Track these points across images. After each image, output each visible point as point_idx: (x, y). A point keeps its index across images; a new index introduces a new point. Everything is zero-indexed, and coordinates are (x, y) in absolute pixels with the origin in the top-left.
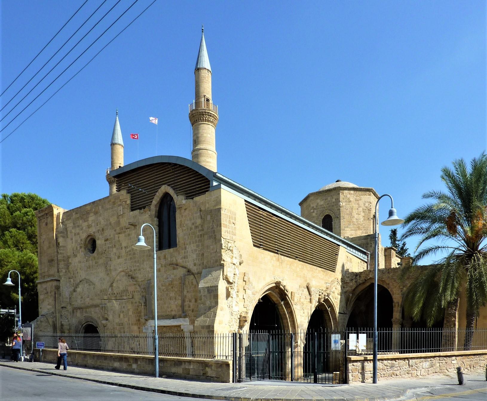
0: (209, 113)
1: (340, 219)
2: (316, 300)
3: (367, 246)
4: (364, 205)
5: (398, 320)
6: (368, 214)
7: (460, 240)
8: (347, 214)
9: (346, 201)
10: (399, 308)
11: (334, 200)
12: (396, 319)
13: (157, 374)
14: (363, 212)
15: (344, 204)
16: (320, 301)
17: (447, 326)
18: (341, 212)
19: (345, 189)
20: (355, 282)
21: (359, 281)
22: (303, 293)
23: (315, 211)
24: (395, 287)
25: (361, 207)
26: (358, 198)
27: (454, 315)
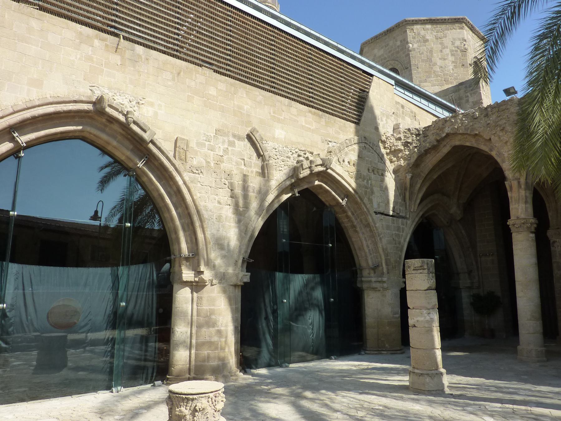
1: (411, 70)
4: (453, 44)
5: (523, 222)
6: (463, 58)
9: (419, 41)
10: (523, 192)
11: (398, 43)
12: (518, 218)
13: (198, 318)
14: (452, 55)
15: (416, 46)
16: (298, 175)
18: (411, 57)
19: (415, 23)
21: (424, 144)
22: (230, 148)
24: (506, 143)
25: (447, 48)
26: (440, 34)
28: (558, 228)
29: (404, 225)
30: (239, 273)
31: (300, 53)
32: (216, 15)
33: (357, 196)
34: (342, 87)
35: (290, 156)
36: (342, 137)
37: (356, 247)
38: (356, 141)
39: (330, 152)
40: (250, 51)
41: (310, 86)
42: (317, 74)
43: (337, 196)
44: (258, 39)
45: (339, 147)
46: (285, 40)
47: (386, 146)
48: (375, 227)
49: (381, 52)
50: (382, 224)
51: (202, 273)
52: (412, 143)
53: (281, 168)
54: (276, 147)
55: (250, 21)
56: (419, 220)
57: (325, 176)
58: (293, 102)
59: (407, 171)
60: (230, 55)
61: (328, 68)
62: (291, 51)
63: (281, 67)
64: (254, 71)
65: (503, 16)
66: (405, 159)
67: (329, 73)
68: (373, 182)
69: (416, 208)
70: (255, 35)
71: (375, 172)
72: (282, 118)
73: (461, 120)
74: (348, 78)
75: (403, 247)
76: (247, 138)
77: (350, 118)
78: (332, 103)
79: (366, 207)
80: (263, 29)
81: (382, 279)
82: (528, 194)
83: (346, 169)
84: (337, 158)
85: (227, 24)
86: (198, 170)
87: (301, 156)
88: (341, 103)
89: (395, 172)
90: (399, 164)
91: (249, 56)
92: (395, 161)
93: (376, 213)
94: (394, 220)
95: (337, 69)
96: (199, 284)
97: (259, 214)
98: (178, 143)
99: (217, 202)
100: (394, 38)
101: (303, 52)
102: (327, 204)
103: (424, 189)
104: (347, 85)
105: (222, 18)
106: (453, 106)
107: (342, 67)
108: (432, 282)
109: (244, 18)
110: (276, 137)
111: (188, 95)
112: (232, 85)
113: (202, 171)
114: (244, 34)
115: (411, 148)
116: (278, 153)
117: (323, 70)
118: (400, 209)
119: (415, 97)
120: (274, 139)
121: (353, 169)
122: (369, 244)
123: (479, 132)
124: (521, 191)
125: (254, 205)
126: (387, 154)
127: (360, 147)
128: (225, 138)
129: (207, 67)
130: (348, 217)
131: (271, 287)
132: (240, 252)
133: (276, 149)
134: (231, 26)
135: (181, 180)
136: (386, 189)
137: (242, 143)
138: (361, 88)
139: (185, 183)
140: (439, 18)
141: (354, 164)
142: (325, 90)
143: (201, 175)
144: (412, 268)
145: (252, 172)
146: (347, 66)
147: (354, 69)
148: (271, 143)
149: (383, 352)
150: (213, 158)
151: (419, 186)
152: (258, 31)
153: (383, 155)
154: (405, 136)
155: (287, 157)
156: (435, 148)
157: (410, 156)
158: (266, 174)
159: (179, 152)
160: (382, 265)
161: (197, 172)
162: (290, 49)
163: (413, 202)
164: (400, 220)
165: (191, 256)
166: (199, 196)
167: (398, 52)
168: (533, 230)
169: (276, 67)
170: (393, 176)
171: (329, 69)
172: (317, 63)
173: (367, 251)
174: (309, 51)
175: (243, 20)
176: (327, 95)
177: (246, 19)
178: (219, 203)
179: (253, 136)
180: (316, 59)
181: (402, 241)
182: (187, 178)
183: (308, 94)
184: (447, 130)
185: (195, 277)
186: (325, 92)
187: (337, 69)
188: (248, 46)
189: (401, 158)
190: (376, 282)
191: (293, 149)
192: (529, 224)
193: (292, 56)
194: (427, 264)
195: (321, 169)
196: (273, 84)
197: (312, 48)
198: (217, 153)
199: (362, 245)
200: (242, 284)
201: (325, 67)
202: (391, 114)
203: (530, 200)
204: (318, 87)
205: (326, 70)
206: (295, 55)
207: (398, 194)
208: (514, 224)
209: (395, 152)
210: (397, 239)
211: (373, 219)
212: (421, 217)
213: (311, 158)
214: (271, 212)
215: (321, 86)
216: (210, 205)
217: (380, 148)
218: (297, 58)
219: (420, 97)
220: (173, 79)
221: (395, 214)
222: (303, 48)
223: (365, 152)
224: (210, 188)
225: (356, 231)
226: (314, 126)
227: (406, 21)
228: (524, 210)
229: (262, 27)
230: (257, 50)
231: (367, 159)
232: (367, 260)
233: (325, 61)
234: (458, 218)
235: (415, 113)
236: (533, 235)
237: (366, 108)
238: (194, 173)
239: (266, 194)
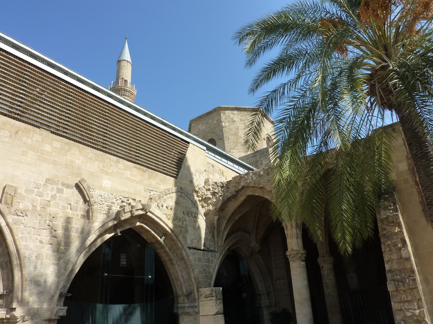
0: (124, 89)
1: (224, 141)
3: (257, 164)
5: (296, 253)
7: (371, 124)
8: (232, 135)
10: (294, 230)
11: (215, 122)
12: (292, 250)
15: (227, 124)
16: (120, 218)
17: (388, 249)
18: (224, 132)
21: (226, 194)
22: (58, 195)
27: (395, 220)
28: (324, 256)
29: (213, 257)
30: (54, 308)
31: (130, 124)
32: (59, 90)
33: (173, 235)
34: (164, 150)
35: (115, 202)
36: (163, 187)
38: (174, 191)
39: (151, 199)
40: (86, 119)
41: (137, 148)
42: (144, 139)
43: (156, 235)
44: (95, 110)
45: (159, 195)
46: (118, 113)
47: (199, 195)
48: (189, 260)
49: (204, 127)
50: (195, 257)
51: (14, 309)
52: (218, 193)
54: (102, 195)
55: (89, 97)
56: (226, 252)
57: (145, 218)
58: (121, 160)
59: (215, 214)
60: (67, 121)
61: (153, 136)
62: (122, 122)
63: (113, 133)
64: (89, 134)
65: (262, 106)
66: (213, 205)
67: (154, 139)
68: (188, 223)
69: (223, 243)
70: (92, 108)
71: (189, 215)
72: (111, 171)
73: (252, 177)
74: (169, 144)
75: (212, 276)
76: (75, 186)
77: (169, 173)
78: (155, 162)
79: (181, 243)
80: (99, 104)
81: (194, 305)
82: (298, 232)
83: (164, 212)
84: (157, 204)
85: (68, 98)
86: (24, 213)
87: (124, 202)
88: (163, 161)
89: (206, 215)
90: (209, 208)
91: (85, 123)
92: (206, 206)
93: (190, 248)
94: (204, 254)
95: (160, 136)
96: (10, 321)
97: (79, 251)
98: (6, 189)
99: (38, 242)
100: (213, 118)
101: (132, 123)
102: (149, 241)
104: (168, 149)
105: (64, 93)
106: (251, 167)
107: (165, 135)
108: (220, 307)
109: (84, 95)
110: (103, 186)
111: (23, 150)
112: (66, 144)
113: (27, 214)
114: (82, 107)
115: (218, 196)
116: (103, 200)
117: (149, 137)
118: (210, 244)
119: (223, 160)
120: (101, 188)
121: (171, 213)
122: (184, 275)
123: (264, 186)
124: (293, 229)
125: (75, 244)
126: (200, 201)
127: (177, 195)
128: (54, 186)
129: (44, 129)
130: (166, 252)
131: (91, 319)
132: (57, 286)
133: (101, 196)
134: (71, 99)
135: (4, 222)
136: (199, 228)
137: (70, 191)
138: (180, 151)
139: (8, 225)
140: (242, 107)
141: (171, 209)
142: (150, 151)
143: (26, 218)
144: (204, 296)
145: (77, 215)
146: (169, 135)
147: (174, 137)
148: (97, 191)
150: (40, 202)
151: (224, 225)
152: (95, 105)
153: (196, 202)
154: (213, 188)
155: (112, 203)
156: (234, 197)
157: (216, 203)
158: (91, 217)
159: (6, 197)
160: (194, 293)
161: (21, 215)
162: (122, 120)
163: (220, 239)
164: (210, 253)
165: (5, 293)
166: (20, 236)
167: (215, 128)
168: (303, 259)
169: (109, 133)
170: (205, 218)
171: (154, 136)
172: (144, 132)
173: (182, 280)
174: (138, 122)
175: (83, 96)
176: (151, 155)
177: (86, 96)
178: (41, 242)
179: (81, 185)
180: (144, 129)
181: (211, 270)
182: (10, 220)
183: (135, 154)
184: (242, 184)
185: (7, 314)
186: (150, 153)
187: (160, 136)
188: (85, 115)
189: (210, 204)
190: (189, 307)
191: (118, 196)
192: (301, 255)
193: (123, 125)
194: (216, 292)
195: (141, 212)
196: (104, 145)
197: (140, 121)
198: (44, 199)
199: (178, 276)
200: (57, 318)
201: (150, 135)
202: (203, 171)
203: (300, 236)
204: (143, 149)
205: (151, 137)
206: (126, 125)
207: (208, 232)
208: (291, 255)
209: (205, 200)
210: (207, 269)
211: (187, 253)
212: (228, 250)
213: (133, 204)
214: (94, 249)
215: (154, 149)
216: (31, 245)
217: (194, 196)
218: (127, 127)
219: (227, 159)
220: (11, 137)
221: (206, 248)
222: (133, 120)
223: (181, 199)
224: (33, 229)
225: (173, 264)
226: (138, 178)
227: (220, 107)
228: (296, 243)
229: (99, 102)
230: (104, 120)
231: (183, 204)
232: (181, 288)
233: (151, 130)
234: (257, 250)
235: (223, 171)
236: (303, 263)
237: (183, 166)
238: (18, 216)
239: (88, 234)
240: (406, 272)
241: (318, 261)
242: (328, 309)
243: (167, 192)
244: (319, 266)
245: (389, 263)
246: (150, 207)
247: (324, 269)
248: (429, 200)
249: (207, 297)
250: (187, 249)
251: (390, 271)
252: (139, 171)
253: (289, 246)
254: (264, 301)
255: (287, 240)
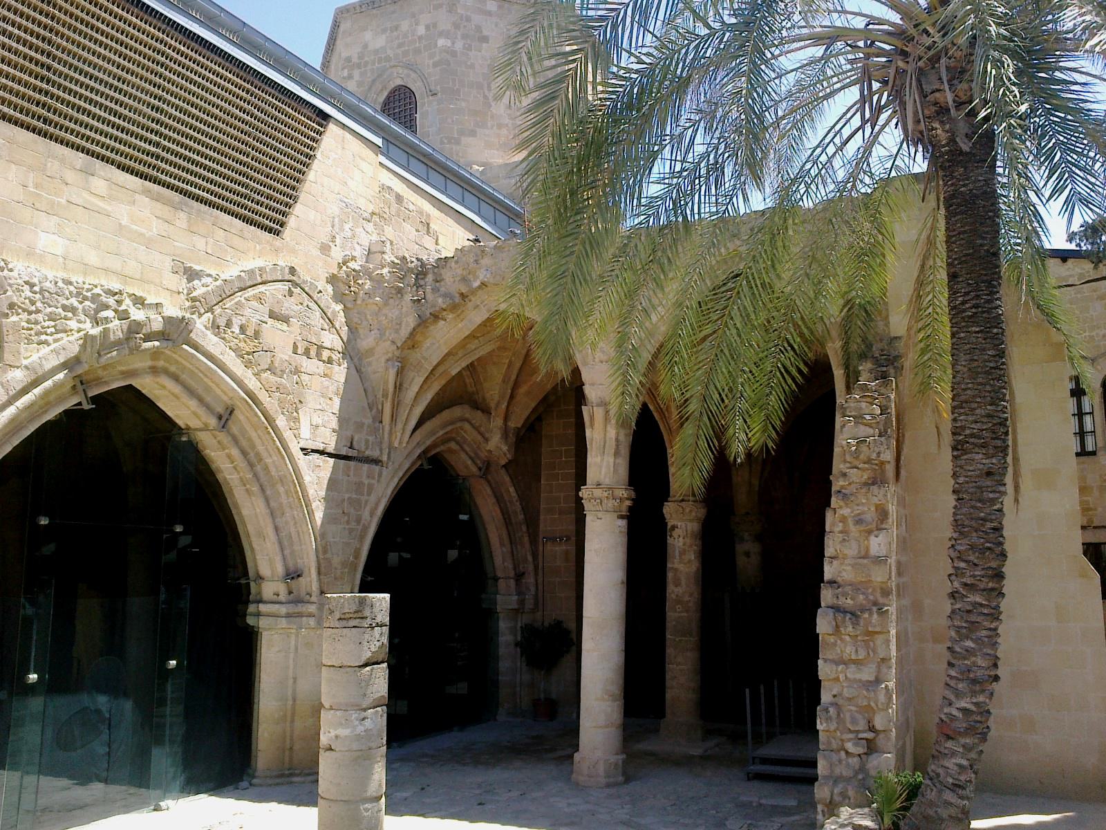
2: (672, 539)
11: (421, 30)
17: (840, 527)
20: (414, 301)
23: (356, 73)
29: (373, 478)
35: (76, 304)
37: (251, 528)
49: (379, 42)
53: (43, 337)
54: (35, 280)
56: (413, 464)
75: (365, 529)
82: (622, 438)
94: (349, 468)
100: (413, 15)
103: (429, 396)
118: (367, 441)
120: (30, 253)
124: (609, 428)
144: (337, 615)
149: (295, 779)
164: (366, 467)
167: (417, 51)
181: (366, 514)
203: (625, 451)
228: (612, 469)
234: (503, 462)
236: (623, 523)
240: (870, 590)
241: (664, 511)
242: (668, 636)
243: (247, 278)
244: (666, 524)
245: (835, 562)
246: (190, 328)
247: (675, 533)
248: (961, 437)
249: (344, 619)
250: (298, 455)
251: (832, 582)
252: (159, 205)
253: (592, 474)
254: (505, 598)
255: (589, 456)
